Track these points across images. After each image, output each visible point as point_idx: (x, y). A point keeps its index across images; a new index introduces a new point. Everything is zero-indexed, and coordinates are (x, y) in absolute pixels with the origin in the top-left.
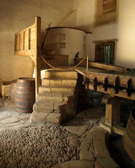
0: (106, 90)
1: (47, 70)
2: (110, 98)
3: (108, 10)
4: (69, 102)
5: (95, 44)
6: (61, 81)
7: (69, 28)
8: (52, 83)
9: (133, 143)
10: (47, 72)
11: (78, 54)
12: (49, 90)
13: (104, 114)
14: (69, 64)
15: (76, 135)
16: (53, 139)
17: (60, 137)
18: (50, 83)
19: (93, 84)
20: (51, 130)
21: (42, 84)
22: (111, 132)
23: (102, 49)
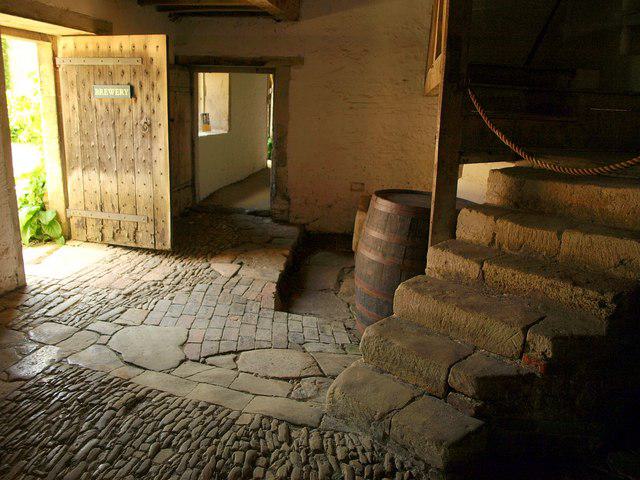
4: (551, 367)
6: (554, 234)
18: (494, 235)
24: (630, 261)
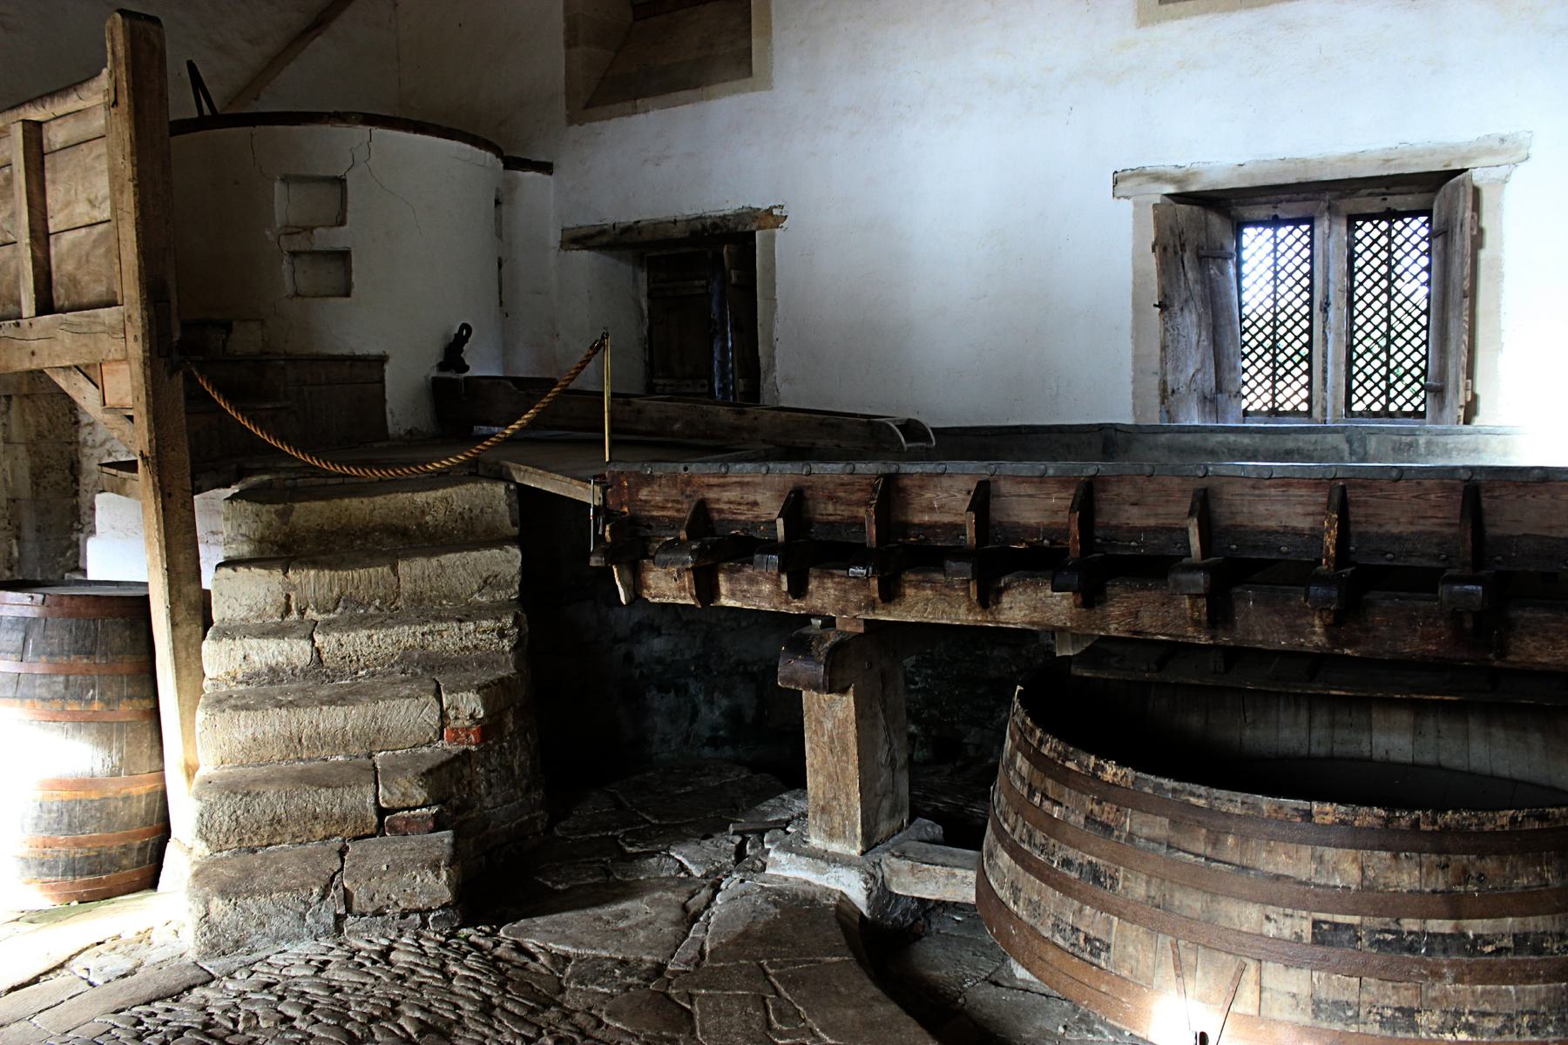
0: (798, 589)
1: (234, 489)
2: (835, 648)
4: (488, 728)
6: (386, 569)
9: (1081, 910)
10: (248, 507)
11: (465, 339)
12: (296, 651)
13: (795, 779)
14: (390, 431)
15: (623, 963)
16: (466, 1029)
17: (509, 1006)
18: (288, 597)
19: (692, 553)
20: (413, 972)
21: (216, 616)
22: (868, 897)
24: (496, 576)
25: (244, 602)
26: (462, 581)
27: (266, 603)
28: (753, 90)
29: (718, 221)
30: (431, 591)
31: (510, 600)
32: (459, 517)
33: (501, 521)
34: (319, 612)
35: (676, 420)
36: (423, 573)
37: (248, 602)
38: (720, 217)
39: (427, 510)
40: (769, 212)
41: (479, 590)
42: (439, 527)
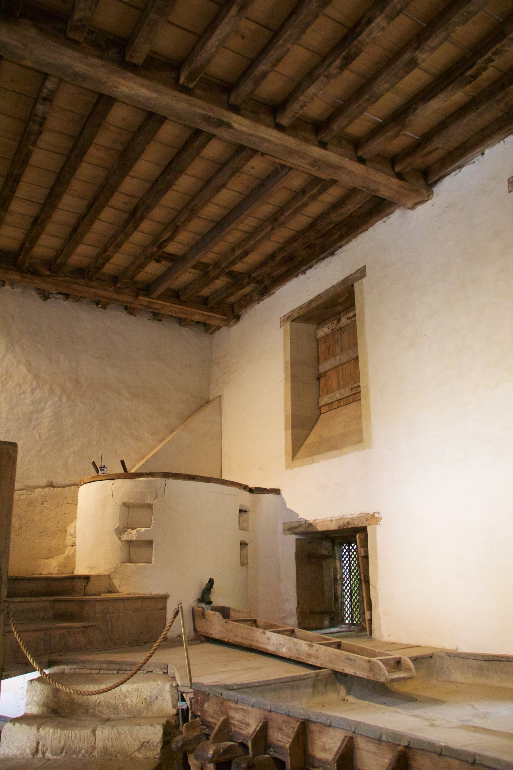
3: (338, 396)
5: (294, 537)
7: (166, 475)
8: (48, 742)
10: (38, 686)
18: (38, 743)
23: (326, 557)
24: (148, 742)
25: (16, 745)
26: (129, 743)
27: (27, 746)
28: (364, 449)
29: (350, 520)
30: (112, 748)
31: (154, 758)
32: (144, 701)
33: (167, 705)
34: (53, 755)
35: (284, 646)
36: (109, 736)
37: (18, 745)
38: (351, 518)
39: (127, 695)
40: (373, 515)
41: (138, 750)
42: (133, 706)
